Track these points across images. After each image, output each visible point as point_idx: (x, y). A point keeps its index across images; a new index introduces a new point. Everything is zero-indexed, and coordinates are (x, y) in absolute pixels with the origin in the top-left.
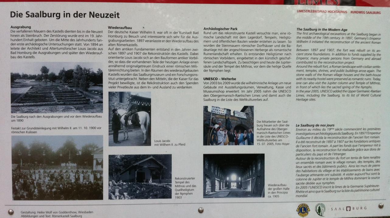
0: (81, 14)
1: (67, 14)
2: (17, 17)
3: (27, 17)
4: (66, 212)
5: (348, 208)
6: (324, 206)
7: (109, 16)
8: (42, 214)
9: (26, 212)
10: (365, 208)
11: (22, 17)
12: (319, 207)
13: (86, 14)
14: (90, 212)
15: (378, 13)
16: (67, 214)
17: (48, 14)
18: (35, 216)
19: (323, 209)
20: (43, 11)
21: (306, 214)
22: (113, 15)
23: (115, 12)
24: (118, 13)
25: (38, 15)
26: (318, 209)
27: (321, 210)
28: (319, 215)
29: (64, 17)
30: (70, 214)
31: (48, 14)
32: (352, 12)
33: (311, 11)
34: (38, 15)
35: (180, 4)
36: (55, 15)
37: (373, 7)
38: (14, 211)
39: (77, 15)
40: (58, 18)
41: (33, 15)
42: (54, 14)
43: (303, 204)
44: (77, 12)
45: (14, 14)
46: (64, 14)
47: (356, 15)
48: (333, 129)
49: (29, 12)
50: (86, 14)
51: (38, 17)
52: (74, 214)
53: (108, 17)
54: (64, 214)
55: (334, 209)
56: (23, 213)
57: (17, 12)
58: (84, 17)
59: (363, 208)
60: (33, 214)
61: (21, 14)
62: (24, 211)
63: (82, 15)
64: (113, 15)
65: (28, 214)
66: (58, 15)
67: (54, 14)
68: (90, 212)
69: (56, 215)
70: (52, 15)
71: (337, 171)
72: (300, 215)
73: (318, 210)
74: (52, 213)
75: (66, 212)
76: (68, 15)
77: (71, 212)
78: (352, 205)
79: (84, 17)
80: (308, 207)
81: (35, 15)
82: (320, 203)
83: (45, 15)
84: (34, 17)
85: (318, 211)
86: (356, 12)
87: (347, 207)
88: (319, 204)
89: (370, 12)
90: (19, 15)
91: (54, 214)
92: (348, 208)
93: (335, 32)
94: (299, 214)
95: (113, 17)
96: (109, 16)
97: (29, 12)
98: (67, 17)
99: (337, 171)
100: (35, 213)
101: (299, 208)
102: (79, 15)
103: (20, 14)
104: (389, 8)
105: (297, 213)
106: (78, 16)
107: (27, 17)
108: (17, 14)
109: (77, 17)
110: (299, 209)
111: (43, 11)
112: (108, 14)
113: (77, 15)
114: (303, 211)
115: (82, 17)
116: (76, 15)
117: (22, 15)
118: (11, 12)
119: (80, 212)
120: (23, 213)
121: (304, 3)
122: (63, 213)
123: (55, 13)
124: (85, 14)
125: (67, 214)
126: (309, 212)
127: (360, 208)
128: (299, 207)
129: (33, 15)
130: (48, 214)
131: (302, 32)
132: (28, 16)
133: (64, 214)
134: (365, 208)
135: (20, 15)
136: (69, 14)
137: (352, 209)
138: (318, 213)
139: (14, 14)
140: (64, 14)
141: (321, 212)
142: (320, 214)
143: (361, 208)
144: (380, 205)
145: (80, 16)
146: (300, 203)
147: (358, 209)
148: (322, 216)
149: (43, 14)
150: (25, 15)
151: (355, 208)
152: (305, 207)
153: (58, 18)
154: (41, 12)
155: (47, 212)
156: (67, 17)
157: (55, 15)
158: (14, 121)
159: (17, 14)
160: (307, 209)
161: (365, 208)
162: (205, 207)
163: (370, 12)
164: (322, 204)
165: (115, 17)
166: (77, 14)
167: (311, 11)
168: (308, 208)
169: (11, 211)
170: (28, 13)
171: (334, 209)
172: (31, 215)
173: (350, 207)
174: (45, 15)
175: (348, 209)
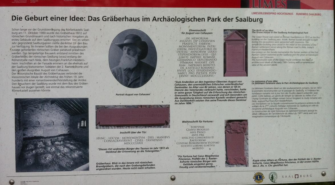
1: (57, 18)
2: (17, 20)
3: (236, 21)
6: (276, 174)
10: (311, 176)
11: (22, 20)
15: (319, 14)
17: (253, 19)
19: (275, 176)
20: (249, 17)
21: (261, 181)
22: (53, 19)
23: (186, 17)
24: (47, 16)
25: (246, 20)
26: (271, 177)
27: (274, 177)
28: (272, 181)
29: (143, 21)
31: (39, 17)
36: (259, 20)
38: (15, 181)
40: (261, 22)
42: (258, 19)
43: (258, 173)
44: (75, 16)
45: (15, 18)
46: (143, 18)
48: (302, 113)
50: (233, 18)
51: (246, 21)
58: (232, 21)
59: (309, 176)
64: (53, 19)
67: (44, 18)
70: (256, 20)
73: (271, 177)
76: (203, 19)
79: (232, 21)
80: (263, 175)
81: (243, 19)
82: (273, 171)
84: (242, 21)
85: (271, 179)
90: (19, 19)
94: (255, 181)
95: (230, 21)
97: (238, 17)
101: (255, 176)
102: (77, 19)
103: (81, 18)
104: (331, 12)
105: (254, 180)
106: (227, 20)
107: (236, 21)
108: (17, 17)
109: (226, 21)
110: (255, 177)
111: (249, 17)
114: (258, 179)
115: (121, 21)
117: (22, 18)
118: (89, 17)
121: (257, 6)
123: (259, 19)
124: (232, 19)
126: (264, 179)
127: (306, 176)
128: (255, 175)
132: (237, 20)
135: (20, 19)
136: (204, 19)
137: (299, 176)
138: (272, 180)
139: (15, 18)
140: (143, 18)
141: (274, 179)
142: (273, 181)
143: (307, 176)
144: (323, 173)
145: (62, 19)
146: (256, 172)
147: (304, 176)
148: (274, 182)
150: (235, 20)
152: (260, 175)
153: (261, 22)
154: (247, 17)
157: (259, 20)
158: (177, 103)
159: (17, 17)
160: (262, 177)
161: (311, 176)
162: (176, 175)
164: (274, 173)
166: (226, 19)
169: (12, 181)
170: (237, 18)
175: (297, 176)
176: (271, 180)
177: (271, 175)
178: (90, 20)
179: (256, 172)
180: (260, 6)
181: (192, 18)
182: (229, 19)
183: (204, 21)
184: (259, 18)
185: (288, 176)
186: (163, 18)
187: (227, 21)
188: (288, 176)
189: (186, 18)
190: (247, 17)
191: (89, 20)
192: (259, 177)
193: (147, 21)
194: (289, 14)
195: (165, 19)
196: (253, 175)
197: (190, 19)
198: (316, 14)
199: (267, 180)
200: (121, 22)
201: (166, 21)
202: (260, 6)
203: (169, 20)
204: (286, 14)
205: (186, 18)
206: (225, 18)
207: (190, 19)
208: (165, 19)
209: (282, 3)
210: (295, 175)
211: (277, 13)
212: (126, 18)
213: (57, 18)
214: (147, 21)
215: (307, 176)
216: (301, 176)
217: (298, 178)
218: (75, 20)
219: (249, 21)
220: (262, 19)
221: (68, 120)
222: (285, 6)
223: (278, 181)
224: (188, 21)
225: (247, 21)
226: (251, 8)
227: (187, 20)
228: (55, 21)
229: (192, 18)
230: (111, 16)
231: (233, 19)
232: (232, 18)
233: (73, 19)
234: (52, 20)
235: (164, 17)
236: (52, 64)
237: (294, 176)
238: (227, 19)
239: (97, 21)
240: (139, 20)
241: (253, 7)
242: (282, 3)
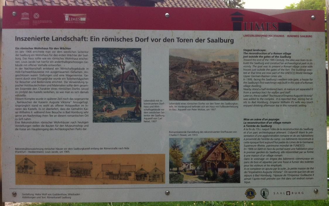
0: (201, 40)
1: (97, 38)
3: (208, 42)
4: (59, 195)
5: (288, 193)
7: (27, 39)
8: (39, 196)
9: (26, 194)
10: (302, 193)
11: (49, 40)
12: (264, 192)
13: (205, 39)
14: (77, 194)
15: (310, 36)
16: (59, 196)
18: (33, 198)
19: (267, 193)
20: (220, 38)
23: (36, 36)
24: (44, 37)
26: (262, 193)
28: (264, 197)
30: (61, 196)
32: (288, 36)
33: (254, 36)
34: (216, 41)
35: (238, 31)
36: (230, 41)
37: (305, 32)
38: (169, 191)
39: (199, 40)
40: (232, 43)
41: (213, 41)
44: (166, 38)
47: (291, 38)
49: (210, 38)
50: (205, 39)
51: (217, 42)
52: (65, 196)
53: (26, 40)
54: (57, 196)
55: (276, 193)
56: (24, 195)
57: (36, 36)
58: (204, 42)
60: (32, 196)
61: (48, 38)
62: (24, 193)
63: (170, 40)
65: (28, 196)
66: (232, 41)
67: (229, 40)
68: (77, 194)
69: (50, 196)
70: (227, 41)
71: (251, 166)
72: (248, 198)
74: (47, 194)
75: (59, 195)
76: (98, 39)
77: (62, 194)
78: (292, 190)
79: (204, 42)
80: (254, 191)
81: (214, 40)
83: (222, 41)
84: (213, 42)
85: (262, 195)
86: (291, 36)
87: (287, 192)
88: (263, 189)
89: (303, 36)
90: (38, 39)
91: (49, 196)
92: (288, 193)
93: (39, 50)
94: (247, 197)
96: (27, 39)
97: (210, 38)
98: (97, 41)
99: (251, 166)
100: (33, 195)
101: (247, 192)
102: (168, 40)
103: (38, 38)
107: (208, 42)
108: (36, 38)
109: (198, 42)
111: (220, 38)
112: (26, 38)
113: (199, 40)
114: (250, 195)
116: (165, 40)
117: (49, 39)
118: (136, 38)
119: (69, 194)
120: (24, 195)
122: (56, 195)
123: (185, 39)
124: (204, 40)
125: (59, 196)
126: (256, 196)
129: (213, 41)
130: (43, 196)
131: (19, 50)
133: (57, 196)
134: (303, 193)
135: (48, 39)
136: (99, 39)
137: (291, 193)
142: (265, 197)
148: (266, 198)
149: (220, 40)
150: (206, 41)
151: (294, 193)
152: (253, 191)
154: (219, 38)
155: (43, 194)
156: (18, 40)
157: (230, 41)
161: (302, 193)
162: (170, 190)
163: (303, 36)
164: (266, 189)
165: (171, 41)
166: (198, 40)
167: (254, 36)
168: (254, 192)
170: (209, 39)
171: (276, 193)
172: (30, 196)
173: (290, 192)
174: (222, 41)
175: (288, 193)
176: (262, 196)
177: (263, 191)
178: (137, 40)
179: (249, 188)
180: (251, 28)
181: (122, 38)
182: (201, 40)
183: (99, 41)
184: (230, 39)
185: (279, 193)
186: (73, 37)
187: (199, 41)
188: (279, 193)
189: (115, 39)
190: (219, 38)
191: (136, 41)
192: (250, 193)
193: (111, 41)
194: (280, 36)
195: (75, 39)
196: (244, 190)
197: (70, 39)
198: (307, 36)
199: (258, 197)
200: (169, 43)
201: (76, 40)
202: (251, 28)
203: (216, 41)
204: (277, 36)
205: (115, 39)
206: (65, 37)
207: (70, 39)
208: (75, 39)
209: (274, 26)
210: (290, 192)
211: (268, 36)
212: (123, 39)
213: (97, 38)
214: (111, 41)
215: (299, 193)
216: (293, 193)
217: (289, 195)
218: (166, 41)
219: (221, 42)
220: (233, 40)
221: (215, 140)
222: (276, 29)
223: (271, 197)
224: (117, 41)
225: (219, 42)
226: (243, 30)
227: (116, 40)
228: (94, 42)
229: (122, 38)
230: (106, 37)
231: (205, 40)
232: (204, 39)
233: (65, 39)
234: (169, 42)
235: (123, 37)
236: (61, 79)
237: (285, 193)
238: (199, 40)
239: (117, 41)
240: (132, 41)
241: (245, 30)
242: (274, 26)
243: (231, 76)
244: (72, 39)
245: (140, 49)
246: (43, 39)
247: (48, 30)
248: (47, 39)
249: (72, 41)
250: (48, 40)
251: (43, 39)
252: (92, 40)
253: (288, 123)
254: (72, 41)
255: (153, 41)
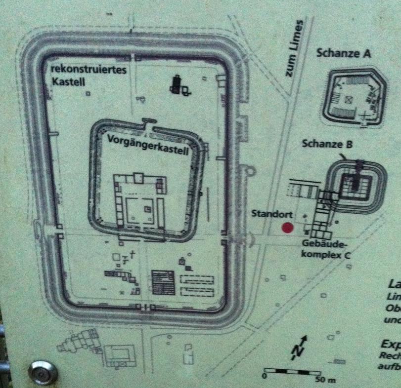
3: (253, 216)
7: (353, 55)
15: (219, 135)
81: (130, 142)
243: (201, 151)
244: (327, 54)
245: (187, 154)
246: (112, 70)
247: (167, 155)
248: (117, 71)
249: (297, 46)
250: (357, 56)
251: (112, 70)
252: (385, 345)
253: (315, 143)
254: (297, 46)
255: (110, 141)
